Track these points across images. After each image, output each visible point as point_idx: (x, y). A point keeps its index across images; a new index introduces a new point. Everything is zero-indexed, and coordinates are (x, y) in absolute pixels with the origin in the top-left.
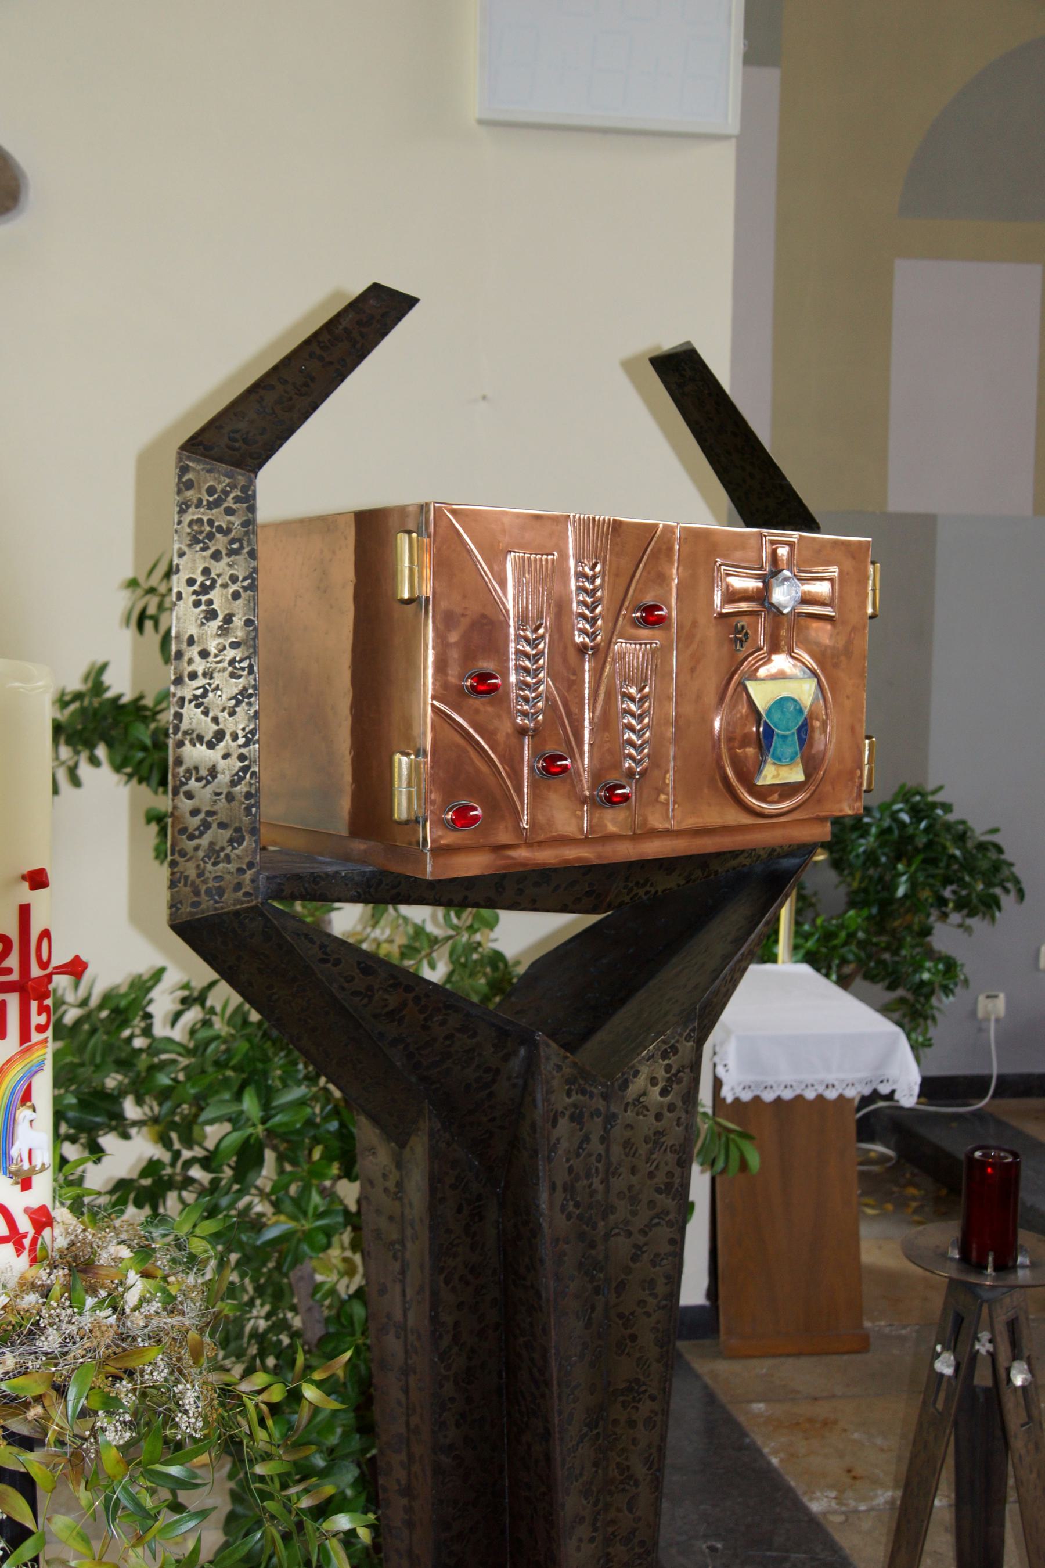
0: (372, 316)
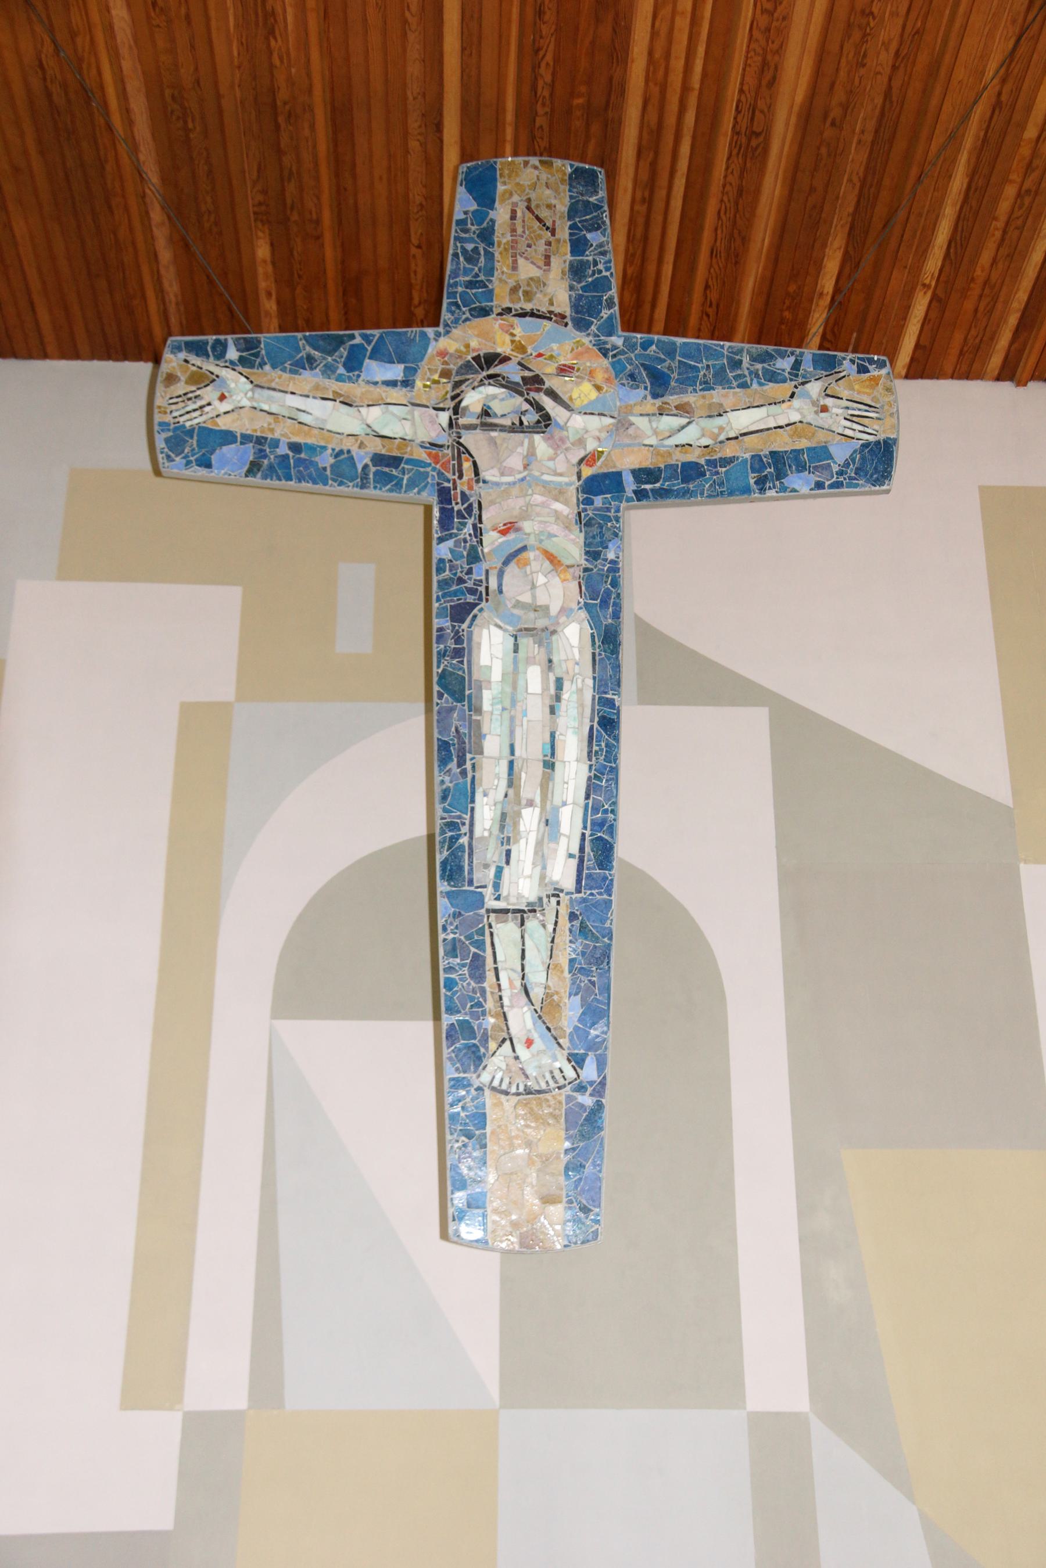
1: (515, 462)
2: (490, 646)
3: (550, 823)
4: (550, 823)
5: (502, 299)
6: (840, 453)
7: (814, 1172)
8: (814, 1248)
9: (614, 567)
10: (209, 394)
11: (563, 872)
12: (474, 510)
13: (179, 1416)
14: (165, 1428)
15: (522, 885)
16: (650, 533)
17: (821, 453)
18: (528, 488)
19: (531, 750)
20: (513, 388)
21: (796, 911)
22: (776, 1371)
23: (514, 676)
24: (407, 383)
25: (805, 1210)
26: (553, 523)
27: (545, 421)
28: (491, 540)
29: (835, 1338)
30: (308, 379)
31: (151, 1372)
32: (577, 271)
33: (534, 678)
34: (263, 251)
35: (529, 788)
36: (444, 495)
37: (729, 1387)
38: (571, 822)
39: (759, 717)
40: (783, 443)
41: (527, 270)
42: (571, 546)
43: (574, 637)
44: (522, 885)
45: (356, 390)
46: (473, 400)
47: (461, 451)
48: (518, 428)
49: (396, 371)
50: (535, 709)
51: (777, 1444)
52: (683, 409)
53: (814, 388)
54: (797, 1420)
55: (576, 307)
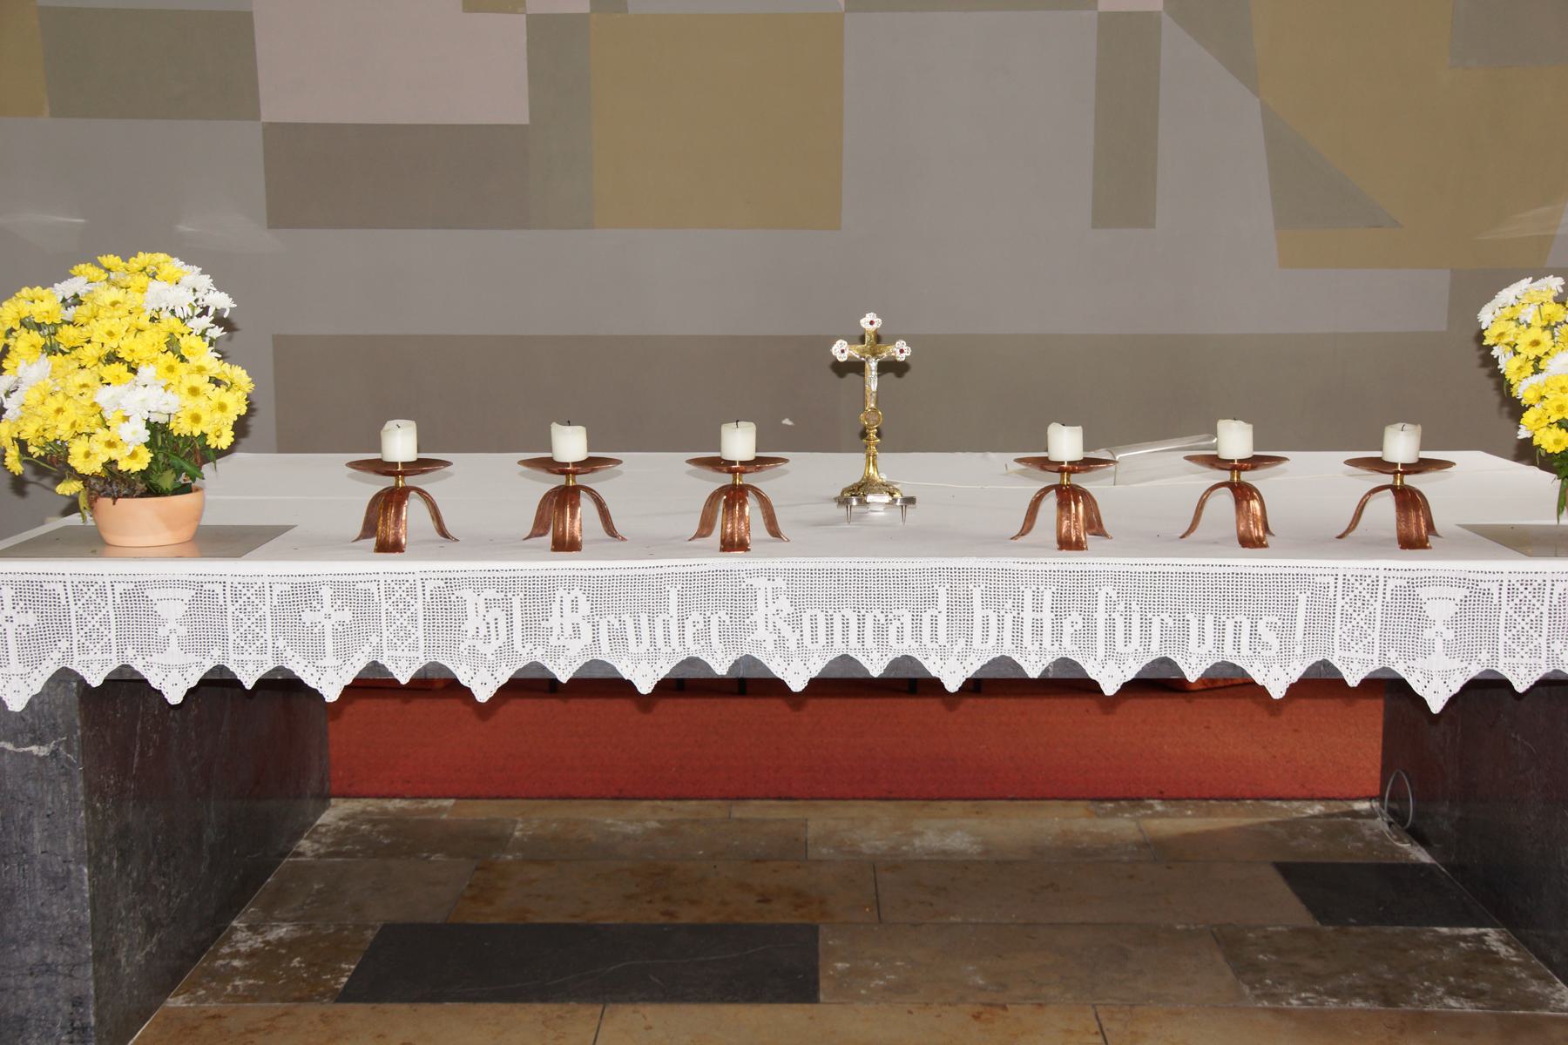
54: (1149, 18)
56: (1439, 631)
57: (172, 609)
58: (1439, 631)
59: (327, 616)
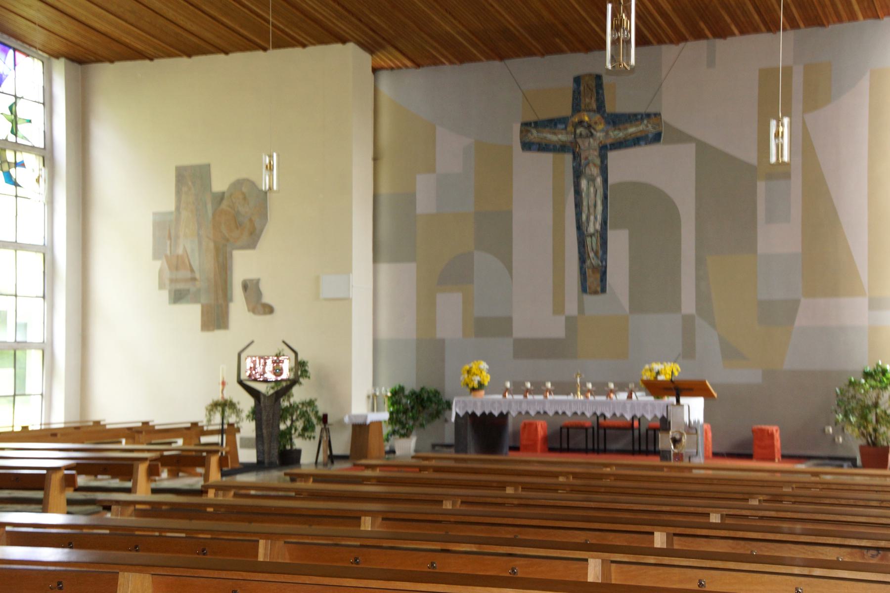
0: (252, 342)
1: (587, 144)
2: (584, 183)
3: (596, 218)
4: (596, 218)
5: (583, 106)
6: (650, 136)
7: (700, 262)
8: (699, 278)
9: (606, 166)
10: (529, 135)
11: (598, 227)
12: (580, 156)
13: (563, 318)
14: (561, 320)
15: (591, 230)
16: (612, 156)
17: (647, 136)
18: (590, 148)
19: (592, 203)
20: (585, 128)
21: (699, 198)
22: (688, 305)
23: (588, 189)
24: (566, 128)
25: (697, 270)
26: (594, 156)
27: (592, 135)
28: (583, 161)
29: (702, 298)
30: (547, 129)
31: (558, 307)
32: (597, 100)
33: (592, 189)
34: (557, 40)
35: (592, 210)
36: (574, 154)
37: (677, 307)
38: (599, 217)
39: (691, 148)
40: (639, 135)
41: (587, 100)
42: (598, 161)
43: (599, 180)
44: (591, 230)
45: (556, 131)
46: (578, 131)
47: (577, 143)
48: (587, 137)
49: (563, 126)
50: (592, 195)
51: (688, 323)
52: (620, 129)
53: (645, 122)
55: (598, 108)
56: (628, 410)
57: (479, 404)
58: (628, 410)
59: (496, 405)
